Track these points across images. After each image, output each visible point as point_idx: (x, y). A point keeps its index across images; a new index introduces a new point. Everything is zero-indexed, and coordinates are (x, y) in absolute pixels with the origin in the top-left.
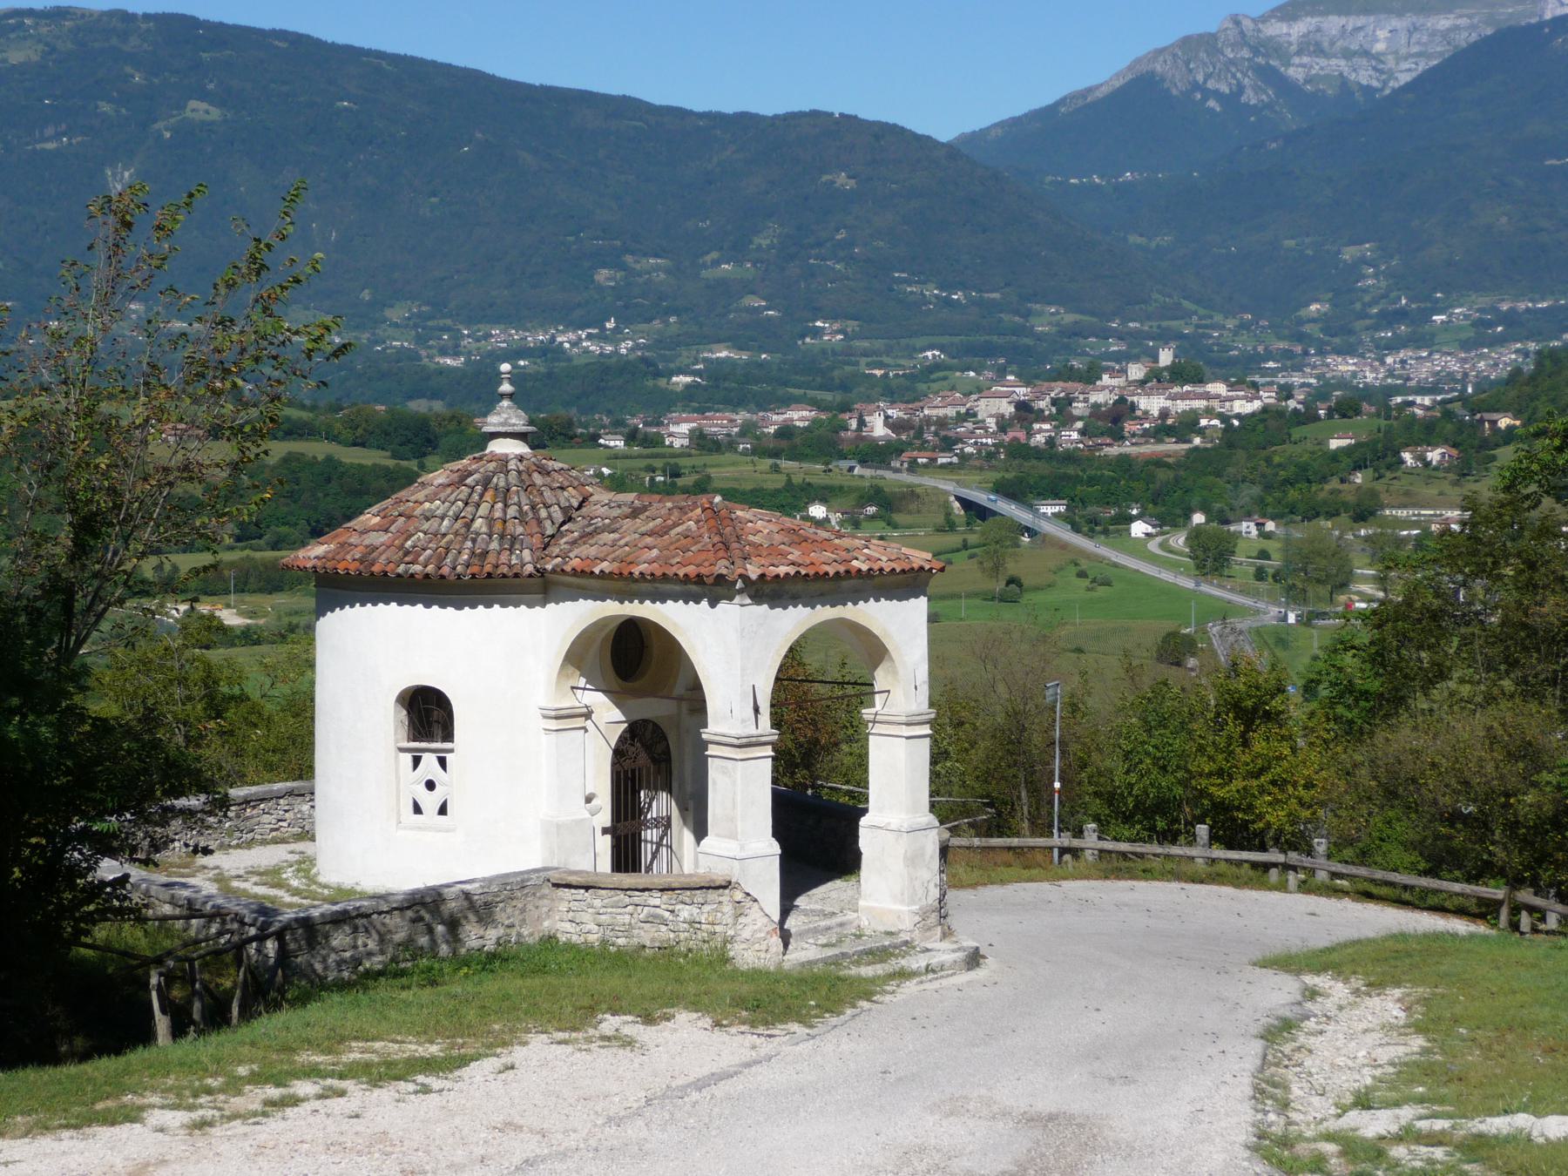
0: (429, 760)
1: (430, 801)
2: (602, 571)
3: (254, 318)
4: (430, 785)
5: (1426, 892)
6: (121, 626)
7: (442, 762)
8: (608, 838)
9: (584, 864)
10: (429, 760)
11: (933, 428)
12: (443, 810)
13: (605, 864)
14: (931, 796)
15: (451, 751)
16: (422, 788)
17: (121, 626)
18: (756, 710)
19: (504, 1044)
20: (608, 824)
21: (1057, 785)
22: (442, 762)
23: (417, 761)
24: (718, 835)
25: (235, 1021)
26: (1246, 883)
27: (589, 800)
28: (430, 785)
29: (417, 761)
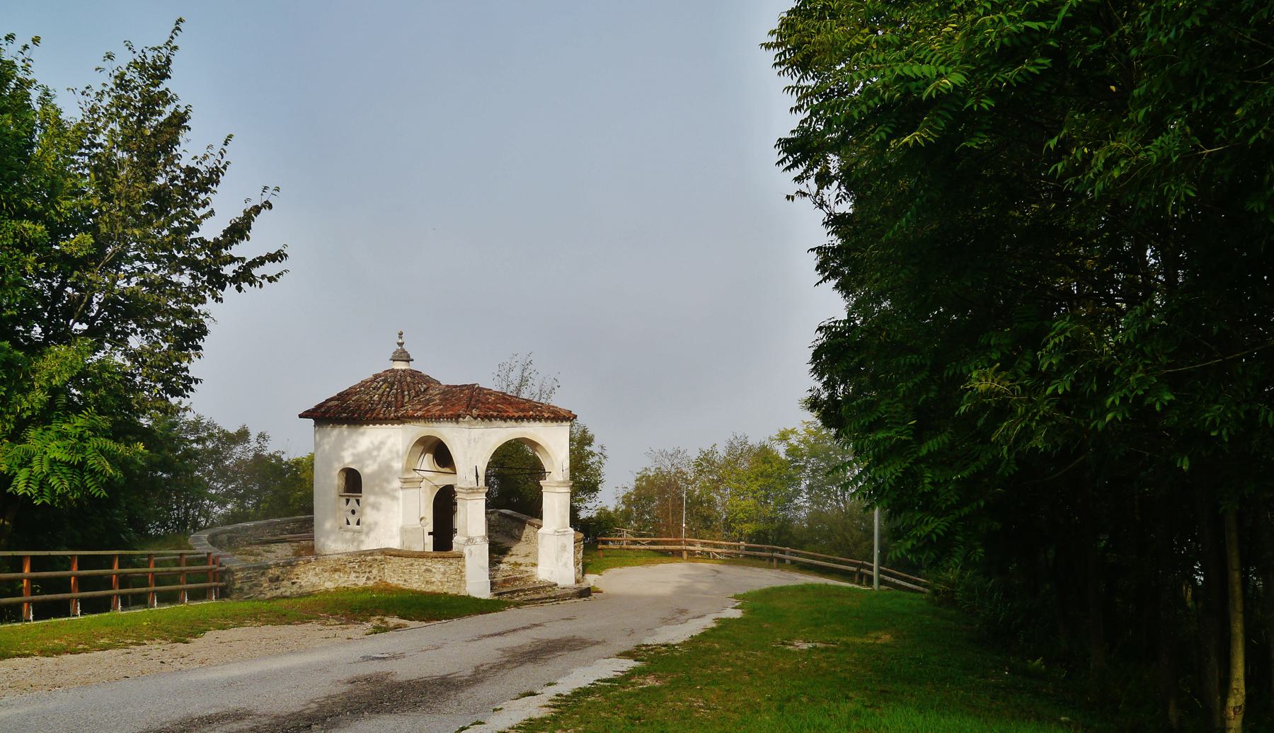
0: (353, 501)
1: (353, 519)
4: (353, 512)
5: (852, 563)
6: (701, 465)
7: (358, 501)
8: (432, 536)
9: (418, 548)
10: (353, 501)
11: (215, 289)
12: (358, 523)
14: (312, 520)
15: (361, 496)
16: (350, 513)
17: (701, 465)
18: (477, 476)
20: (432, 531)
22: (358, 501)
23: (348, 501)
24: (461, 534)
25: (881, 567)
28: (353, 512)
29: (348, 501)
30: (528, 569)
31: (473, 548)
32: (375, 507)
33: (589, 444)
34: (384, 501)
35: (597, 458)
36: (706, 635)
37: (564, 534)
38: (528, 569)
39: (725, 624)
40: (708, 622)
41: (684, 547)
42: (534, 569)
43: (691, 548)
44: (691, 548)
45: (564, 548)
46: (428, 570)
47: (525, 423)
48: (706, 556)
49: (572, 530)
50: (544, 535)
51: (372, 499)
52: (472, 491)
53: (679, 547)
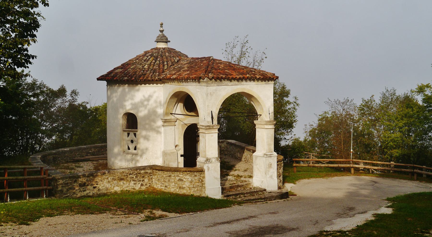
0: (132, 134)
1: (132, 146)
2: (173, 78)
3: (376, 132)
7: (135, 135)
8: (183, 158)
9: (174, 165)
10: (132, 134)
13: (181, 165)
16: (130, 142)
19: (277, 196)
20: (183, 154)
21: (352, 150)
22: (135, 135)
23: (128, 134)
24: (202, 156)
26: (322, 177)
27: (176, 146)
28: (132, 141)
29: (128, 134)
30: (247, 179)
31: (210, 165)
32: (146, 138)
33: (287, 96)
34: (152, 134)
35: (292, 106)
36: (368, 225)
37: (270, 156)
38: (247, 179)
39: (380, 218)
40: (369, 216)
41: (352, 165)
42: (250, 180)
43: (357, 166)
44: (357, 166)
45: (270, 166)
46: (180, 180)
47: (244, 82)
48: (367, 172)
49: (275, 154)
50: (257, 157)
51: (144, 133)
52: (209, 128)
53: (348, 165)
